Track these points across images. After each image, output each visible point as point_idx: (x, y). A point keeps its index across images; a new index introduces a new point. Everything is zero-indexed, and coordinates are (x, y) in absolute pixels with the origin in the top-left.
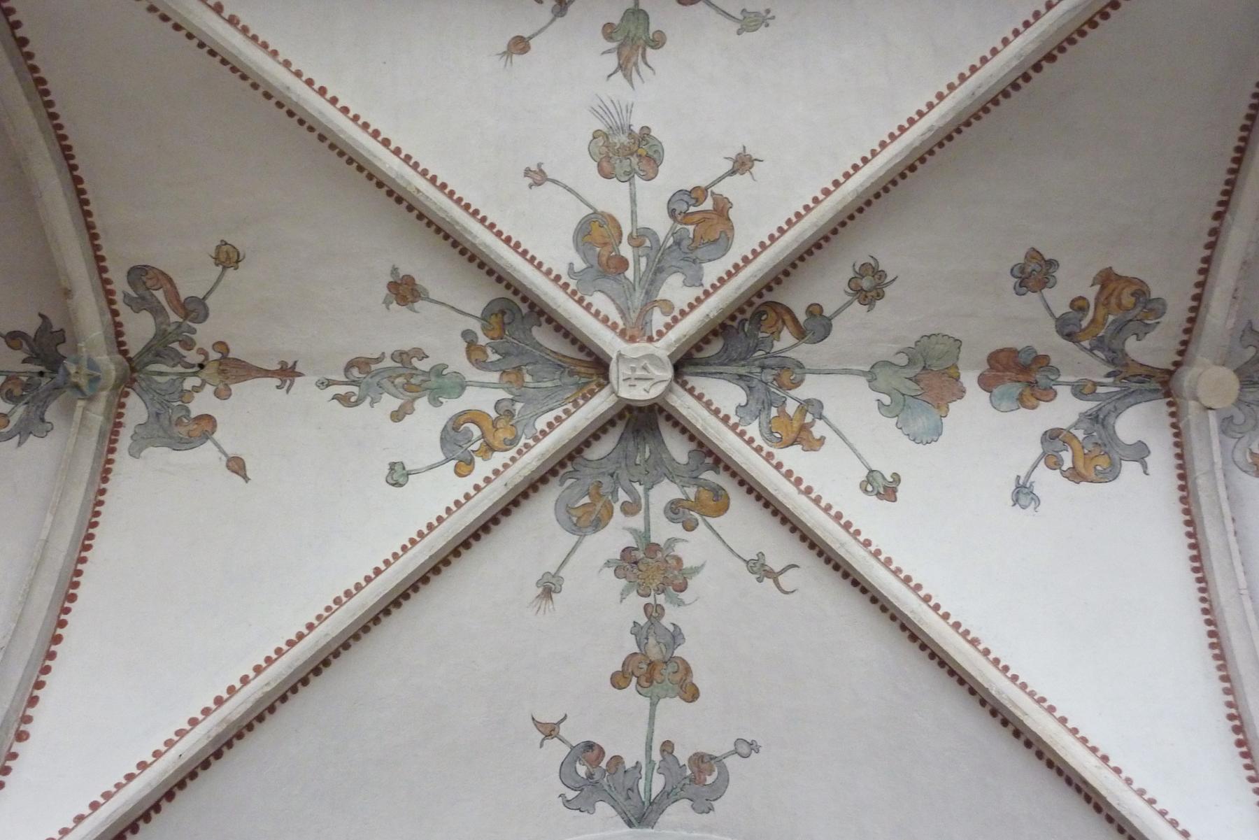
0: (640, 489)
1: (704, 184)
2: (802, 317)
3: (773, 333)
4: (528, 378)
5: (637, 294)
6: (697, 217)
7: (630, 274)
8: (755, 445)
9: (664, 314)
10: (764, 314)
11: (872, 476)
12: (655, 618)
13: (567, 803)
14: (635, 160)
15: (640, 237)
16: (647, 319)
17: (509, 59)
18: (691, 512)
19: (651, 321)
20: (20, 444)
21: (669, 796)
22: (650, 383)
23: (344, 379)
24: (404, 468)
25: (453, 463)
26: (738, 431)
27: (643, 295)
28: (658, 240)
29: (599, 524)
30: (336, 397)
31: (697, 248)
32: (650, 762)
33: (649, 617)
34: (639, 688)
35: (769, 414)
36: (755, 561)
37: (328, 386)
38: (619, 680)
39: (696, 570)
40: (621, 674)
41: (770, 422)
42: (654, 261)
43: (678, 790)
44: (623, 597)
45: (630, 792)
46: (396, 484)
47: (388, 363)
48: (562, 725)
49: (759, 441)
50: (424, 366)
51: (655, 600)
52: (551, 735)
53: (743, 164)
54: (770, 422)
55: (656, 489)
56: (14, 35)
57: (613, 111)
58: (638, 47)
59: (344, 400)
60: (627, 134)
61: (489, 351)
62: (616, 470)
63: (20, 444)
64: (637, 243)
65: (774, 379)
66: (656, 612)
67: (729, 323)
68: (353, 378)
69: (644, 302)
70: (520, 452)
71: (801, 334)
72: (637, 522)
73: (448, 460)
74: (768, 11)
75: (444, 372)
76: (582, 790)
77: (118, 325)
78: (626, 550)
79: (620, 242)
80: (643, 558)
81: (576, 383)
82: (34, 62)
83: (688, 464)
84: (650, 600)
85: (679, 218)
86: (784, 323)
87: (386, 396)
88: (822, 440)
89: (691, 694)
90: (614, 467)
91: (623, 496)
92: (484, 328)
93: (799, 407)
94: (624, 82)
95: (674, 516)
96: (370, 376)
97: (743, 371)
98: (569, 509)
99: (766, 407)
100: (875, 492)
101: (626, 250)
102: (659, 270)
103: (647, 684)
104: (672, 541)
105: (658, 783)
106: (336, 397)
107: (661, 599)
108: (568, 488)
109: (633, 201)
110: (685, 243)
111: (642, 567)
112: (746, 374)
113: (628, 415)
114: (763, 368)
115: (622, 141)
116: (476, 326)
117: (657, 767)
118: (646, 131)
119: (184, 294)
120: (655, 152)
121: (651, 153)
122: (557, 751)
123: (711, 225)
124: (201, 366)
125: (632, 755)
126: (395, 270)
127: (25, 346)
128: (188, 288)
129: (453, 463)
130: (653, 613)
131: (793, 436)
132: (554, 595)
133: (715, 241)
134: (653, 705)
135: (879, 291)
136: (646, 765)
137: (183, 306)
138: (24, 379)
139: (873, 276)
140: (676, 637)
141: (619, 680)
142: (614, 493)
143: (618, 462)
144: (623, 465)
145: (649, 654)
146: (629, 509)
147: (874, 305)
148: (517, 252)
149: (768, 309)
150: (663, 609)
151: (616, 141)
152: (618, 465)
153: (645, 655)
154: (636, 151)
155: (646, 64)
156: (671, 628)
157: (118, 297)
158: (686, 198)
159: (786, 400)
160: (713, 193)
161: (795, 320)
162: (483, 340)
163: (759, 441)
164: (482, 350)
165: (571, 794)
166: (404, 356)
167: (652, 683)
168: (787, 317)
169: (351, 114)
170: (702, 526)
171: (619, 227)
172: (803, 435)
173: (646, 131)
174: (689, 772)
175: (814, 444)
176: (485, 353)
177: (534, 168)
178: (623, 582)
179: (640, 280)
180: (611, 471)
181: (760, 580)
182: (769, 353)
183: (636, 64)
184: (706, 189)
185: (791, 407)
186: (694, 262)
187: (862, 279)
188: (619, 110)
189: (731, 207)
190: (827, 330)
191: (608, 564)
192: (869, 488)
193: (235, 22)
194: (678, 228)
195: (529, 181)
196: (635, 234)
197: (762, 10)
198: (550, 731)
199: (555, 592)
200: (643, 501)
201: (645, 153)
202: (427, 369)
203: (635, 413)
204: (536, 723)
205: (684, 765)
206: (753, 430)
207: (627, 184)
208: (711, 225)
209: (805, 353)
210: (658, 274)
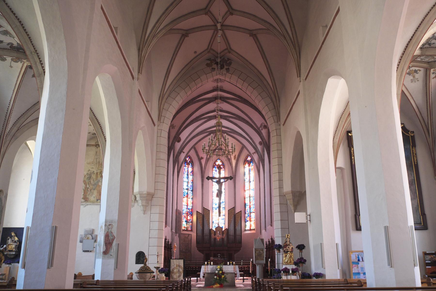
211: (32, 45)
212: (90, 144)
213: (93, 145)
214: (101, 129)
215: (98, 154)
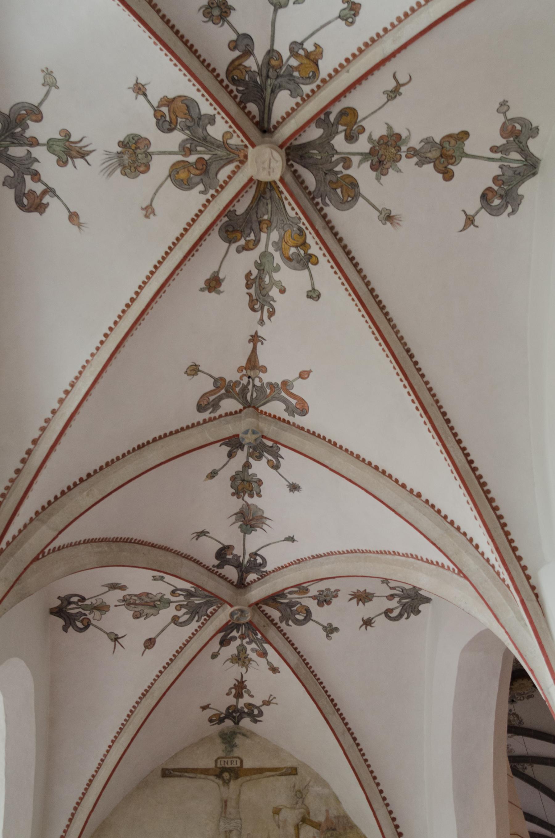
0: (336, 157)
1: (152, 112)
2: (237, 53)
3: (246, 72)
4: (266, 217)
5: (219, 153)
6: (173, 117)
7: (206, 157)
8: (316, 89)
9: (231, 137)
10: (234, 78)
11: (343, 17)
12: (414, 152)
13: (514, 212)
14: (138, 151)
15: (186, 150)
16: (234, 147)
17: (82, 225)
18: (354, 129)
19: (235, 145)
20: (282, 458)
21: (524, 151)
22: (272, 160)
23: (260, 312)
24: (311, 291)
25: (310, 265)
26: (306, 98)
27: (220, 150)
28: (187, 140)
29: (354, 184)
30: (269, 318)
31: (191, 117)
32: (500, 160)
33: (414, 155)
34: (455, 164)
35: (298, 78)
36: (389, 96)
37: (263, 321)
38: (448, 175)
39: (389, 127)
40: (445, 175)
41: (302, 78)
42: (199, 142)
43: (521, 145)
44: (399, 171)
45: (516, 173)
46: (319, 296)
47: (252, 291)
48: (468, 213)
49: (313, 86)
50: (255, 272)
51: (404, 152)
52: (472, 221)
53: (140, 89)
54: (302, 78)
55: (336, 147)
56: (86, 480)
57: (110, 162)
58: (70, 145)
59: (272, 314)
60: (123, 155)
61: (248, 239)
62: (323, 171)
63: (282, 458)
64: (188, 152)
65: (276, 70)
66: (411, 151)
67: (238, 100)
68: (260, 308)
69: (224, 149)
70: (319, 87)
71: (248, 52)
72: (356, 160)
73: (308, 268)
74: (43, 71)
75: (259, 262)
76: (508, 202)
77: (226, 415)
78: (373, 167)
79: (188, 162)
80: (378, 158)
81: (270, 190)
82: (98, 469)
83: (324, 129)
84: (403, 155)
85: (173, 126)
86: (240, 65)
87: (271, 293)
88: (316, 45)
89: (465, 135)
90: (321, 172)
91: (339, 168)
92: (234, 242)
93: (294, 58)
94: (92, 155)
95: (355, 138)
96: (259, 300)
97: (269, 90)
98: (343, 202)
99: (293, 78)
100: (353, 17)
101: (192, 159)
102: (205, 139)
103: (454, 159)
104: (370, 139)
105: (515, 156)
106: (269, 318)
107: (404, 148)
108: (331, 202)
109: (164, 153)
110: (189, 124)
111: (382, 159)
112: (271, 87)
113: (291, 162)
114: (268, 77)
115: (127, 158)
116: (234, 246)
117: (504, 156)
118: (121, 144)
119: (212, 387)
120: (133, 139)
121: (134, 142)
122: (483, 217)
123: (177, 108)
124: (249, 377)
125: (494, 169)
126: (202, 290)
127: (235, 451)
128: (209, 386)
129: (310, 265)
130: (413, 153)
131: (312, 64)
132: (392, 214)
133: (187, 106)
134: (468, 156)
135: (221, 3)
136: (502, 162)
137: (218, 387)
138: (251, 450)
139: (212, 8)
140: (428, 141)
141: (448, 175)
142: (337, 173)
143: (319, 170)
144: (320, 166)
145: (436, 157)
146: (347, 162)
147: (231, 6)
148: (192, 225)
149: (231, 75)
150: (410, 148)
151: (127, 161)
152: (321, 169)
153: (436, 159)
154: (133, 150)
155: (81, 140)
156: (423, 144)
157: (212, 415)
158: (161, 122)
159: (289, 65)
160: (158, 107)
161: (238, 58)
162: (242, 242)
163: (313, 86)
164: (247, 242)
165: (509, 209)
166: (249, 283)
167: (453, 156)
168: (237, 63)
169: (118, 320)
170: (363, 124)
171: (179, 162)
172: (312, 57)
173: (121, 144)
174: (512, 139)
175: (319, 51)
176: (249, 241)
177: (144, 212)
178: (390, 170)
179: (210, 151)
180: (324, 174)
181: (400, 94)
182: (258, 74)
183: (81, 148)
184: (155, 110)
185: (294, 62)
186: (200, 119)
187: (213, 15)
188: (109, 159)
189: (167, 97)
190: (247, 36)
191: (378, 179)
192: (350, 20)
193: (73, 383)
194: (179, 127)
195: (152, 216)
196: (183, 153)
197: (42, 75)
198: (470, 221)
199: (390, 214)
200: (343, 156)
201: (134, 145)
202: (257, 271)
203: (290, 157)
204: (464, 229)
205: (507, 141)
206: (306, 89)
207: (153, 156)
208: (177, 108)
209: (260, 52)
210: (207, 140)
211: (282, 123)
212: (191, 766)
213: (205, 772)
214: (503, 529)
215: (230, 809)
